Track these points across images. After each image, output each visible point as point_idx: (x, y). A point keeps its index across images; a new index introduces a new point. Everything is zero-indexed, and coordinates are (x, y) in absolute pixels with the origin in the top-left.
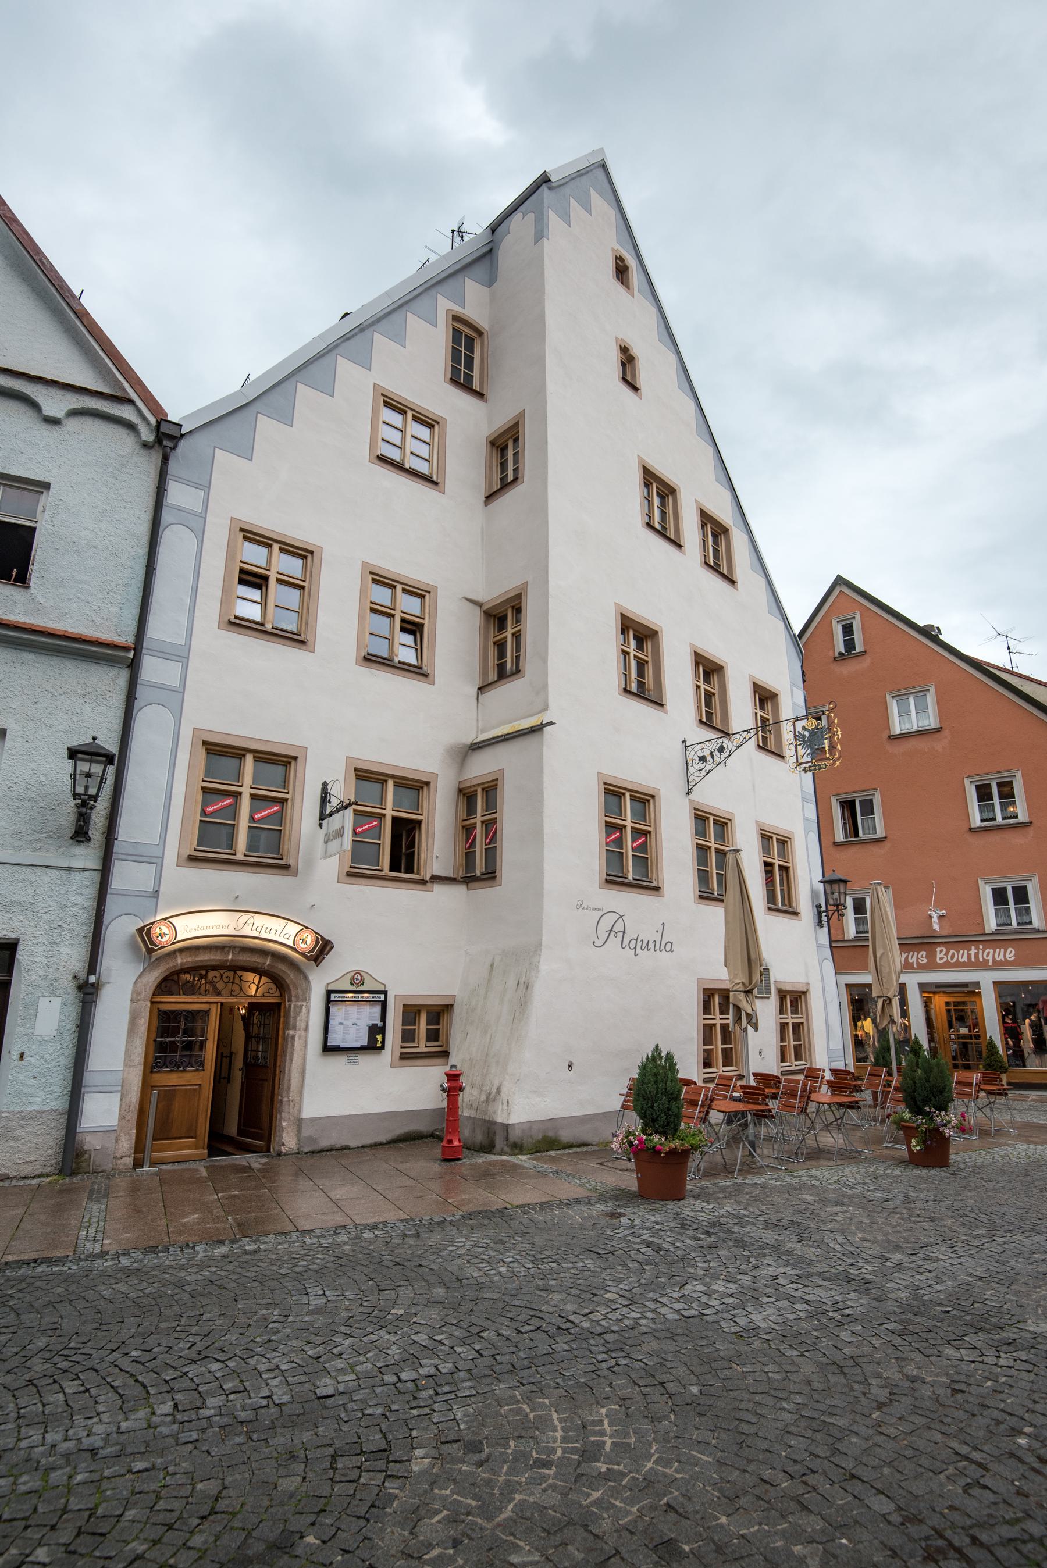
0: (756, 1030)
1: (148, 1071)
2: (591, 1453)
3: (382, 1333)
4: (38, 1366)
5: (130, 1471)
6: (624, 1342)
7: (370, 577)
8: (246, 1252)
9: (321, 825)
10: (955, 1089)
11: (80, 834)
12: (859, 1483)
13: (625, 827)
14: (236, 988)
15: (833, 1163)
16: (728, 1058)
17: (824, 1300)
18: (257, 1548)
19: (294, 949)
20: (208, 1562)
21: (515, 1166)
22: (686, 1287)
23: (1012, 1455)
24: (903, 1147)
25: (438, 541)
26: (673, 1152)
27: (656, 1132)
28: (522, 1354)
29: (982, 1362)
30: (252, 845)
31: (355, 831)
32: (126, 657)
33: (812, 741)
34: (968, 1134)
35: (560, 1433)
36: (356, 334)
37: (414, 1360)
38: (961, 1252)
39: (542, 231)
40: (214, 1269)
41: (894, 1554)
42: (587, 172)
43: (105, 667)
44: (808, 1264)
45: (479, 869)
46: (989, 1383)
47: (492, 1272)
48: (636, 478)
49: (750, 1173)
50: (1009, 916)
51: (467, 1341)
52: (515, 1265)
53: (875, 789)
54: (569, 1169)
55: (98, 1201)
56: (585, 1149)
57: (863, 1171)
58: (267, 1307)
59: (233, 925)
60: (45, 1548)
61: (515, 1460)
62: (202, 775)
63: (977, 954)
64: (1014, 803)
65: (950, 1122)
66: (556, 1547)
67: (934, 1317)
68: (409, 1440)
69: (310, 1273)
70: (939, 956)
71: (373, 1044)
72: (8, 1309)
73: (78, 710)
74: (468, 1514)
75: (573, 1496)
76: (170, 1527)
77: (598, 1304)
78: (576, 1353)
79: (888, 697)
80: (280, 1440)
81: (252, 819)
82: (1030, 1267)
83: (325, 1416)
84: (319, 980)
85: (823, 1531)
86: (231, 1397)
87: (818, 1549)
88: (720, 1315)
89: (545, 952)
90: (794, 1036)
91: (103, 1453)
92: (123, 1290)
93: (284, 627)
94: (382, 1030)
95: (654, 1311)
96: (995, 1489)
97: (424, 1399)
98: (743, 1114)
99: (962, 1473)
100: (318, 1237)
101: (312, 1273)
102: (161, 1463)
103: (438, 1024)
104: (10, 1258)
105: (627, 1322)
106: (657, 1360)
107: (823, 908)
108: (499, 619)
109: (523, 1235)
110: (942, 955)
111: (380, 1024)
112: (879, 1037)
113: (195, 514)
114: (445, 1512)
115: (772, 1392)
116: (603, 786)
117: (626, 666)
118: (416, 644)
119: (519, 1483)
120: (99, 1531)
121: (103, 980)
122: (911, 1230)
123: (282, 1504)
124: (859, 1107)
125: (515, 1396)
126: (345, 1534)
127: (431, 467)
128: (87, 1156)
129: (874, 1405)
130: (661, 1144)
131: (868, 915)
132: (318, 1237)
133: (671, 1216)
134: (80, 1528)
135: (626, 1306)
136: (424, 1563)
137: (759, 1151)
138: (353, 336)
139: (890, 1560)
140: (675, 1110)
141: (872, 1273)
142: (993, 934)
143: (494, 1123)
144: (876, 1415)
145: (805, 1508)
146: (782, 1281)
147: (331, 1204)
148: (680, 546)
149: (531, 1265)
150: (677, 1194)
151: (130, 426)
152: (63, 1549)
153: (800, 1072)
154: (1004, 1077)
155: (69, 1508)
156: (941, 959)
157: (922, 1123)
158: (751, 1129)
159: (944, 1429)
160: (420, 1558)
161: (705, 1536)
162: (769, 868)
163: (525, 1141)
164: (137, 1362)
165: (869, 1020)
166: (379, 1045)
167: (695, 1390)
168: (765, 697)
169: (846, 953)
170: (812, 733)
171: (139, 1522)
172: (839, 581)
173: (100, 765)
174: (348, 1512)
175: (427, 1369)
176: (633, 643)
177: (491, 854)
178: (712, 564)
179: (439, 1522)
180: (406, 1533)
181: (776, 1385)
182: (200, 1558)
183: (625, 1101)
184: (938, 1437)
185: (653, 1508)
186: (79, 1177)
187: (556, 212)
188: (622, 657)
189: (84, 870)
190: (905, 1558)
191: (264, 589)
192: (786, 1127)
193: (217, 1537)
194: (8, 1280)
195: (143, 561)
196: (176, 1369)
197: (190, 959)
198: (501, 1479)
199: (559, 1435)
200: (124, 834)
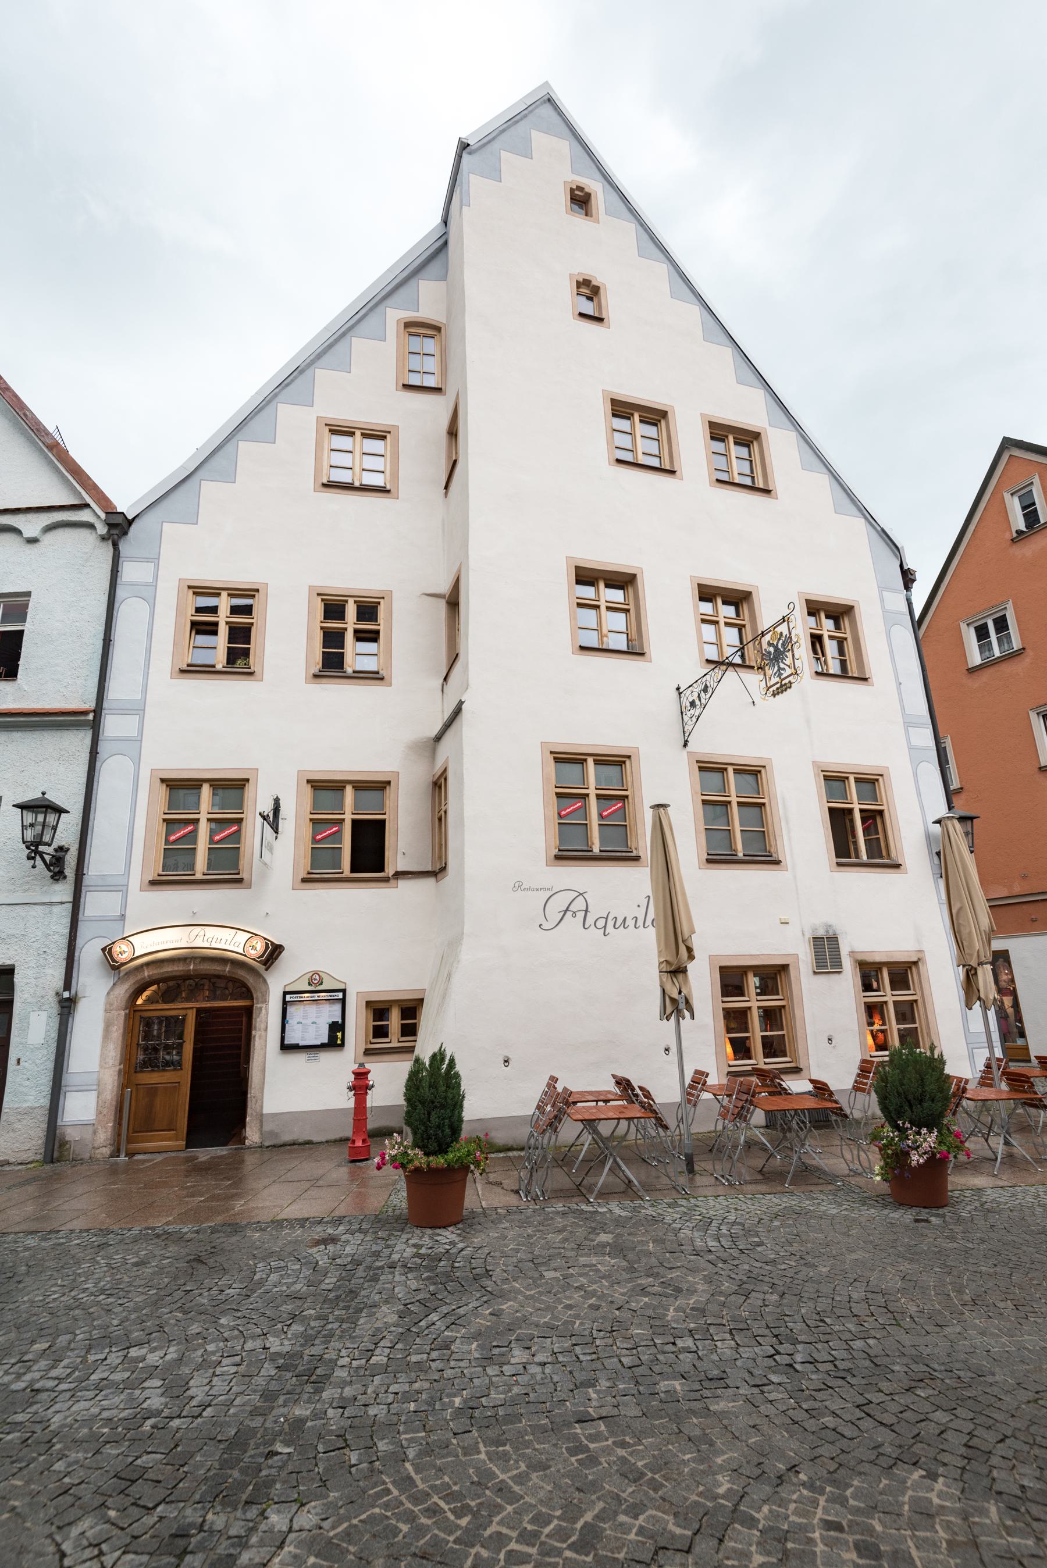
32: (89, 720)
36: (296, 378)
42: (526, 116)
62: (554, 783)
81: (601, 816)
84: (277, 983)
113: (147, 585)
121: (80, 995)
138: (292, 381)
151: (91, 526)
166: (339, 1042)
189: (62, 903)
197: (155, 972)
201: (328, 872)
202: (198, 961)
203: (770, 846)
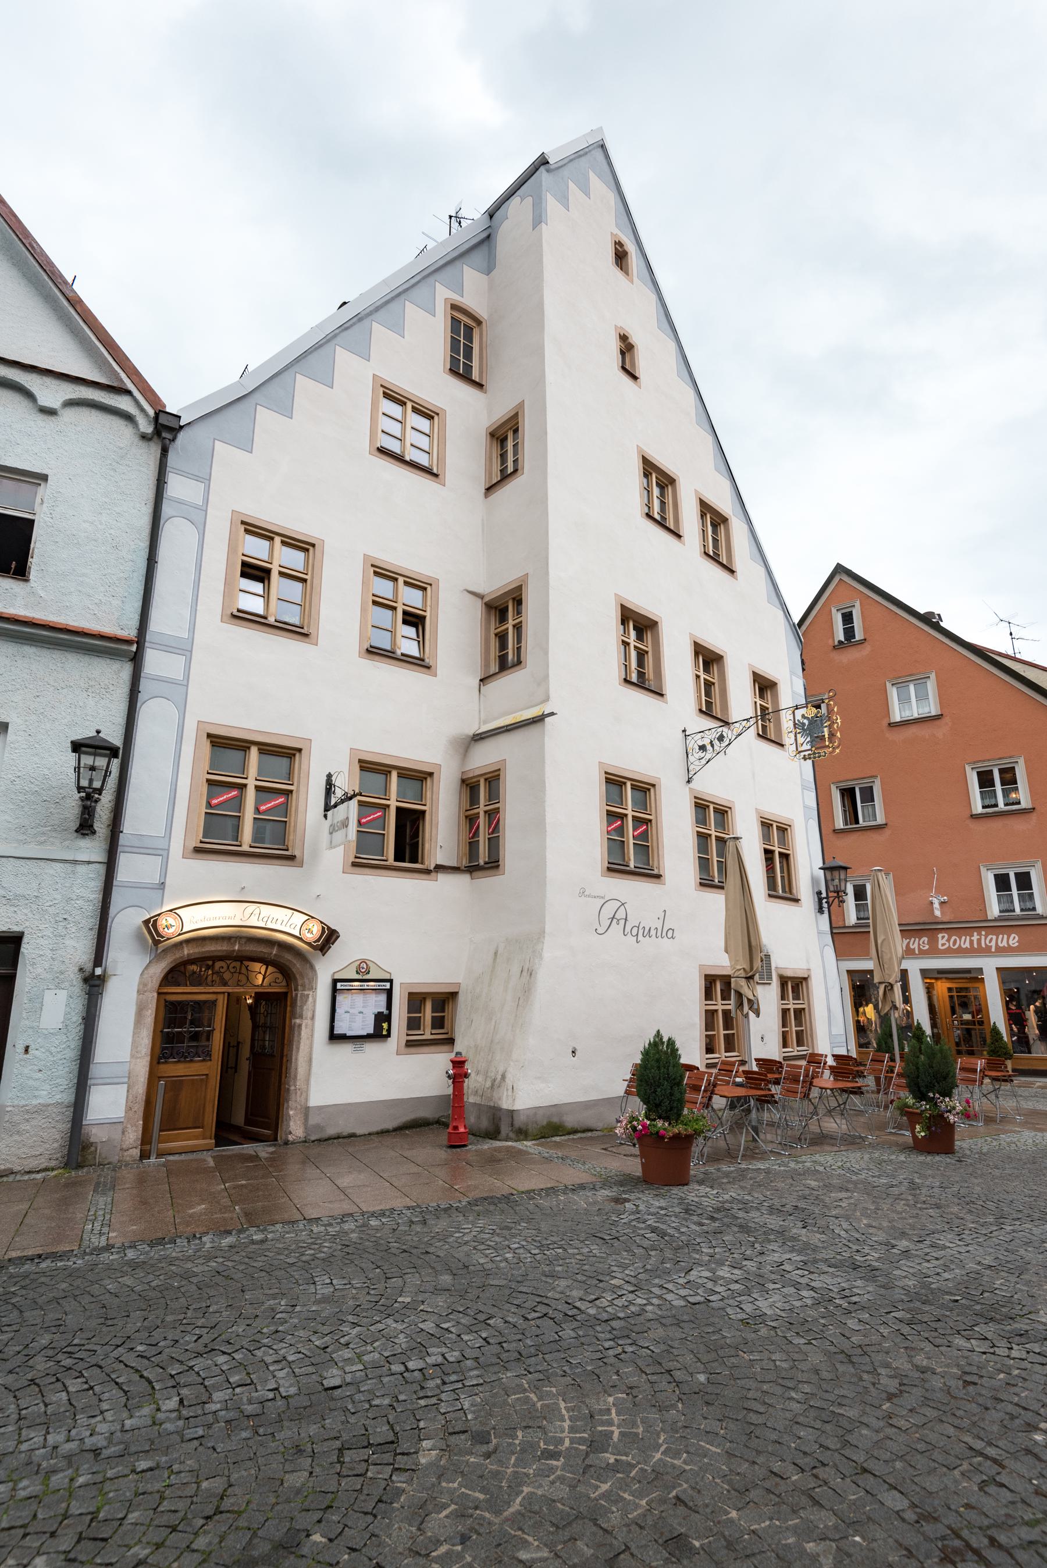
0: (758, 1016)
1: (155, 1062)
2: (598, 1444)
3: (390, 1321)
4: (41, 1364)
5: (133, 1471)
6: (630, 1329)
7: (372, 569)
8: (253, 1242)
9: (325, 816)
10: (959, 1075)
11: (85, 827)
12: (871, 1478)
13: (626, 815)
14: (243, 978)
15: (836, 1149)
16: (730, 1044)
17: (831, 1287)
18: (262, 1548)
19: (300, 939)
20: (212, 1565)
21: (520, 1152)
22: (692, 1273)
23: (1028, 1451)
24: (907, 1133)
25: (440, 532)
26: (677, 1137)
27: (660, 1118)
28: (529, 1342)
29: (993, 1354)
30: (258, 837)
31: (359, 821)
32: (130, 650)
33: (811, 729)
34: (972, 1120)
35: (568, 1422)
36: (354, 324)
37: (421, 1349)
38: (968, 1239)
39: (541, 216)
40: (221, 1260)
41: (910, 1554)
42: (586, 153)
43: (108, 661)
44: (814, 1250)
45: (483, 857)
46: (1002, 1376)
47: (498, 1259)
48: (636, 468)
49: (753, 1158)
50: (1012, 902)
51: (474, 1328)
52: (521, 1251)
53: (875, 777)
54: (573, 1155)
55: (104, 1194)
56: (589, 1134)
57: (867, 1157)
58: (274, 1297)
59: (239, 916)
60: (44, 1557)
61: (523, 1451)
62: (207, 768)
63: (979, 941)
64: (1017, 789)
65: (954, 1108)
66: (565, 1542)
67: (942, 1306)
68: (416, 1431)
69: (317, 1262)
70: (941, 942)
71: (380, 1032)
72: (10, 1307)
73: (81, 704)
74: (476, 1508)
75: (581, 1488)
76: (174, 1529)
77: (604, 1290)
78: (582, 1340)
79: (888, 685)
80: (287, 1434)
81: (257, 810)
82: (1041, 1256)
83: (332, 1407)
84: (326, 969)
85: (836, 1527)
86: (238, 1390)
87: (831, 1547)
88: (726, 1301)
89: (547, 940)
90: (796, 1022)
91: (106, 1453)
92: (129, 1283)
93: (287, 620)
94: (388, 1018)
95: (660, 1297)
96: (1012, 1488)
97: (432, 1389)
98: (746, 1099)
99: (977, 1470)
100: (325, 1225)
101: (319, 1262)
102: (166, 1462)
103: (443, 1011)
104: (14, 1254)
105: (633, 1308)
106: (663, 1347)
107: (824, 895)
108: (500, 610)
109: (529, 1221)
110: (944, 941)
111: (386, 1012)
112: (881, 1023)
113: (196, 507)
114: (453, 1507)
115: (780, 1381)
116: (604, 775)
117: (627, 657)
119: (527, 1475)
120: (101, 1536)
121: (109, 972)
122: (917, 1216)
123: (288, 1501)
124: (862, 1093)
125: (522, 1385)
126: (353, 1531)
127: (431, 459)
128: (93, 1149)
129: (884, 1396)
130: (665, 1129)
131: (869, 902)
132: (325, 1225)
133: (676, 1201)
134: (81, 1533)
135: (632, 1292)
136: (432, 1561)
137: (762, 1136)
138: (352, 326)
139: (906, 1560)
140: (677, 1095)
141: (878, 1260)
142: (995, 920)
143: (500, 1109)
144: (886, 1406)
145: (816, 1503)
146: (787, 1267)
147: (338, 1192)
148: (679, 536)
149: (537, 1251)
150: (681, 1179)
151: (128, 418)
152: (62, 1557)
153: (802, 1057)
154: (1009, 1064)
155: (70, 1512)
156: (943, 945)
157: (926, 1109)
158: (754, 1114)
159: (957, 1422)
160: (428, 1555)
161: (715, 1530)
162: (769, 856)
163: (529, 1127)
164: (142, 1357)
165: (871, 1006)
166: (385, 1033)
167: (702, 1378)
168: (764, 686)
169: (846, 939)
170: (812, 721)
171: (142, 1524)
172: (839, 569)
173: (106, 757)
174: (355, 1508)
175: (434, 1358)
176: (633, 634)
177: (494, 843)
178: (711, 553)
179: (447, 1517)
180: (414, 1529)
181: (783, 1374)
182: (204, 1561)
183: (628, 1086)
184: (951, 1431)
185: (663, 1501)
186: (85, 1170)
187: (555, 196)
188: (622, 647)
189: (89, 863)
190: (922, 1560)
191: (266, 582)
192: (788, 1112)
193: (222, 1539)
194: (11, 1276)
195: (144, 554)
196: (182, 1362)
197: (197, 950)
198: (509, 1471)
199: (566, 1424)
200: (129, 826)
201: (373, 858)
202: (244, 940)
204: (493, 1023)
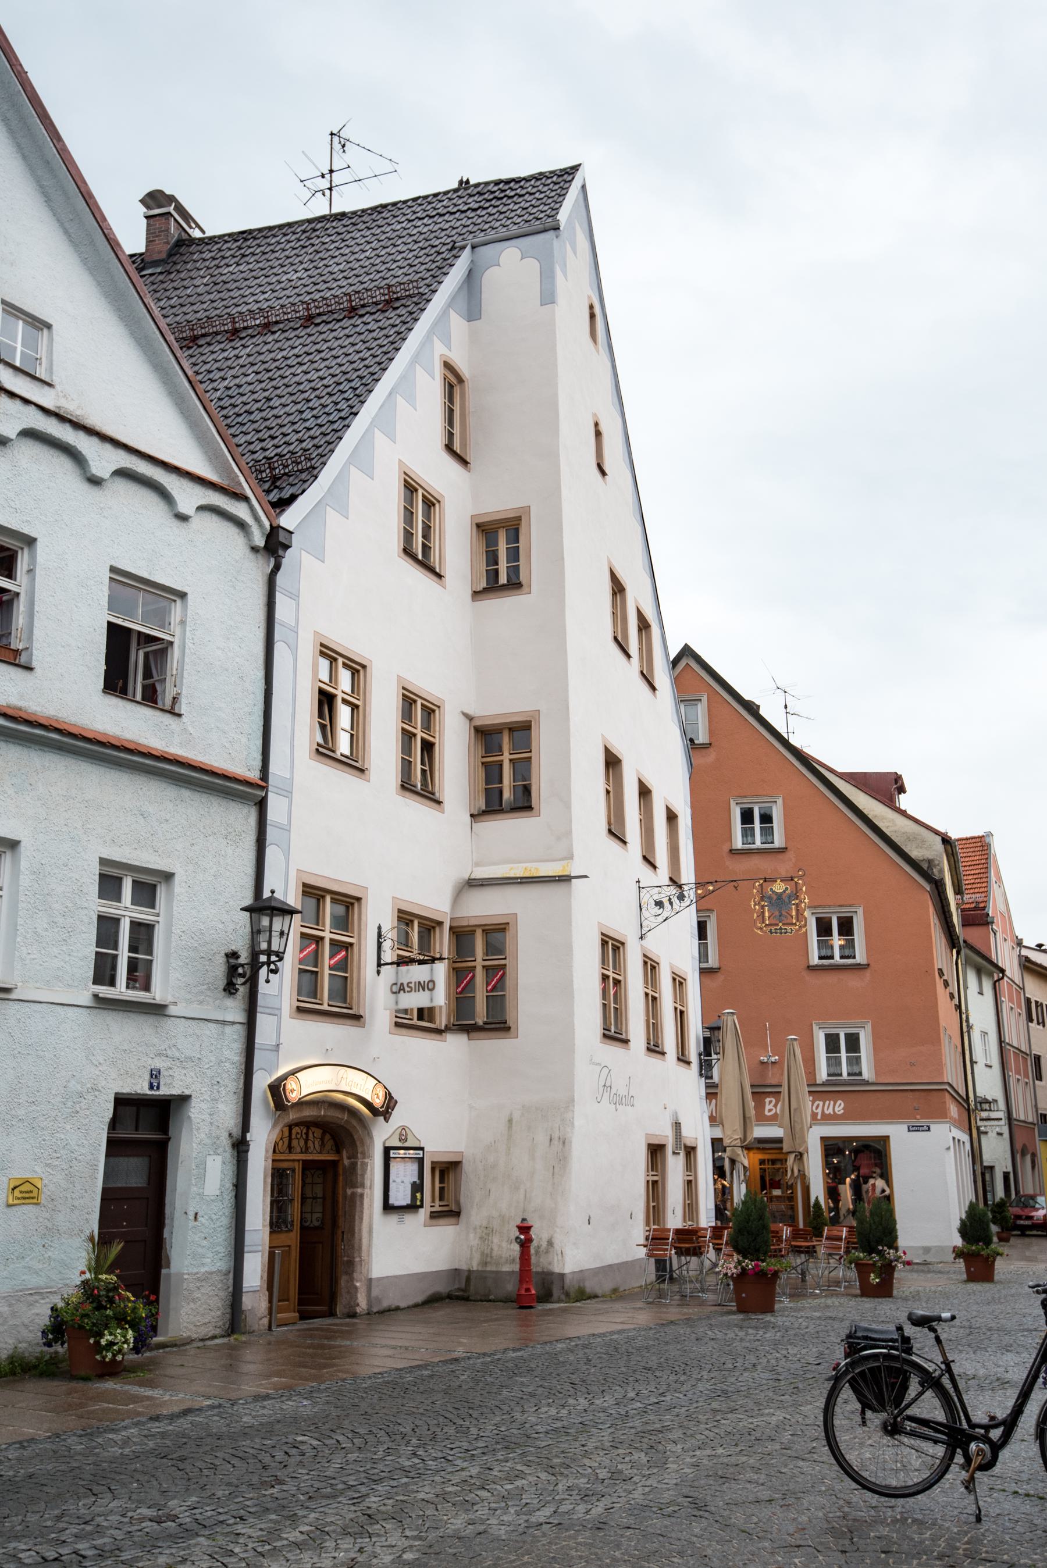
9: (378, 972)
53: (710, 910)
70: (768, 1107)
110: (771, 1106)
118: (352, 729)
142: (823, 1084)
143: (551, 1274)
151: (241, 525)
156: (770, 1110)
189: (233, 1023)
203: (351, 998)
204: (522, 1191)
